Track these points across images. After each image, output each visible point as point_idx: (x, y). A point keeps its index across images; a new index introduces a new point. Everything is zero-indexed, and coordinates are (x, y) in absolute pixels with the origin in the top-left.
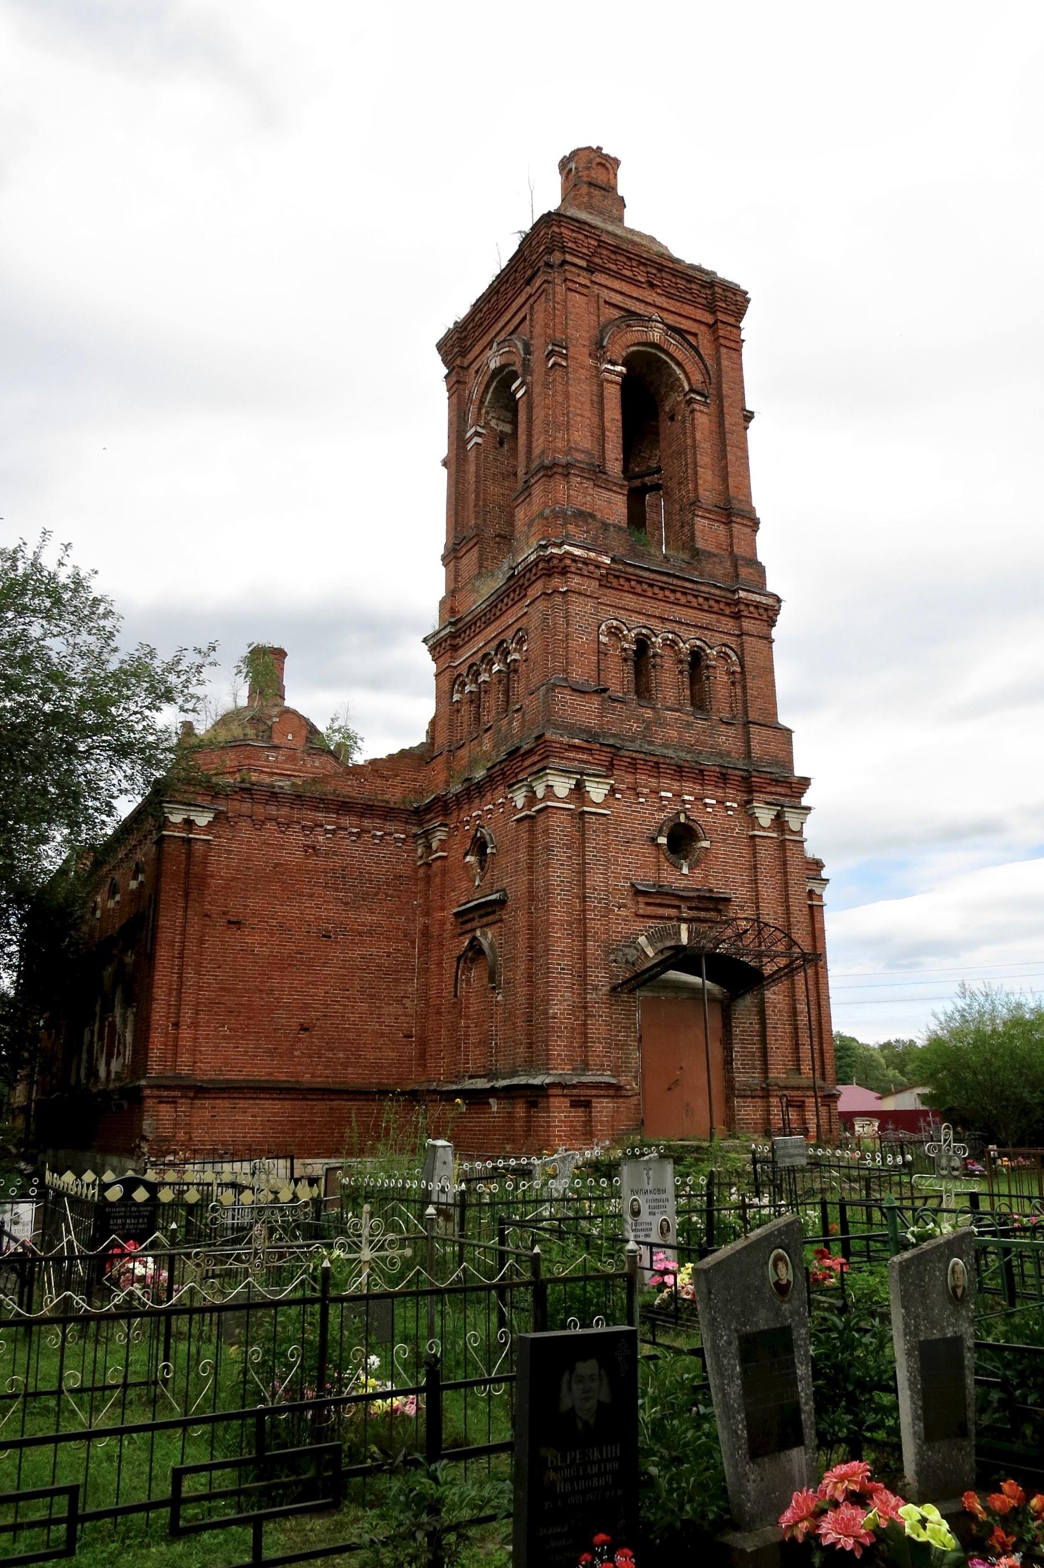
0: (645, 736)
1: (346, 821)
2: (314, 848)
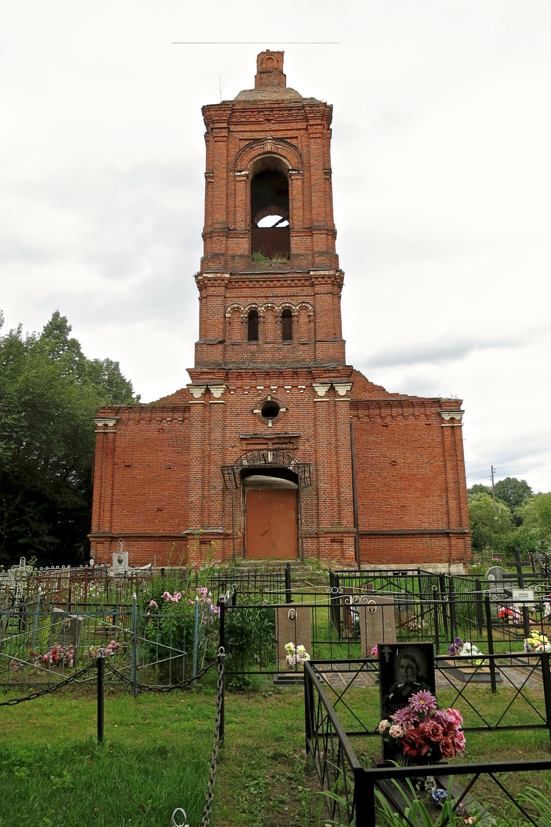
0: (251, 360)
1: (176, 416)
2: (162, 429)
